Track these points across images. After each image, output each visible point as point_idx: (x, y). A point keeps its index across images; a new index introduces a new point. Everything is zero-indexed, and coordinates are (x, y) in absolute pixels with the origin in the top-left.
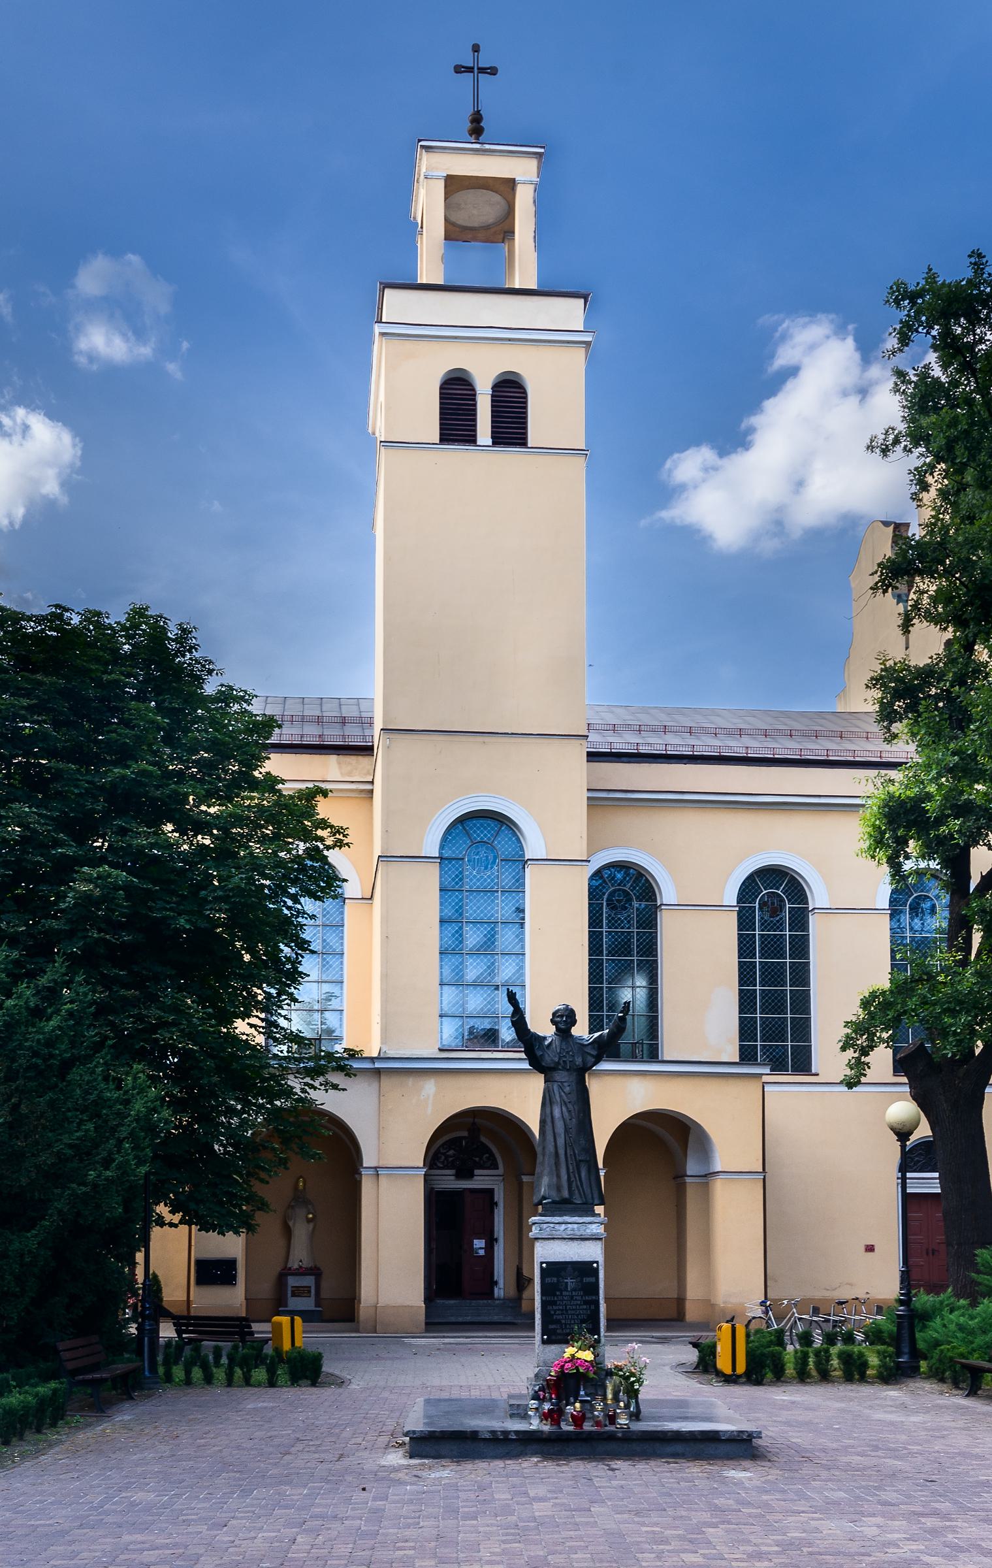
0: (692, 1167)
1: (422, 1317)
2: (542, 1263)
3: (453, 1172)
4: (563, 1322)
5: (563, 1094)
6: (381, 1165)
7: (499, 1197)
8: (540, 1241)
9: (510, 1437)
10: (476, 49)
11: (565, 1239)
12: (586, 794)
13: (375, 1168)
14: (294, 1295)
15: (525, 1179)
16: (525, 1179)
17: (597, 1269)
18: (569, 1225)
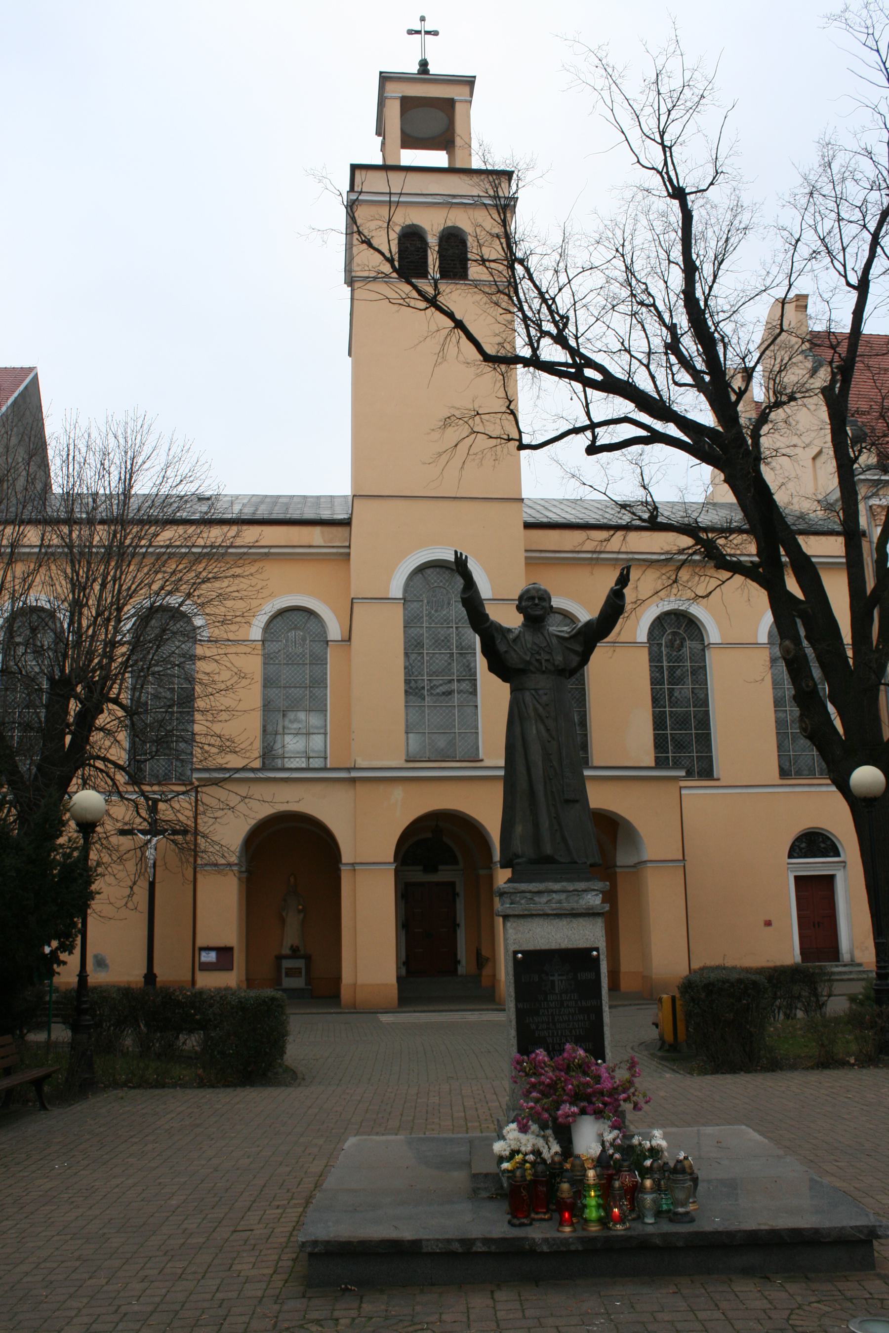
0: (623, 859)
1: (395, 992)
2: (515, 953)
3: (421, 868)
4: (550, 1040)
5: (538, 706)
6: (358, 861)
7: (459, 888)
8: (511, 919)
9: (474, 1249)
10: (423, 19)
11: (548, 915)
12: (524, 554)
13: (353, 864)
14: (287, 975)
15: (482, 872)
16: (482, 872)
17: (597, 959)
18: (554, 895)
